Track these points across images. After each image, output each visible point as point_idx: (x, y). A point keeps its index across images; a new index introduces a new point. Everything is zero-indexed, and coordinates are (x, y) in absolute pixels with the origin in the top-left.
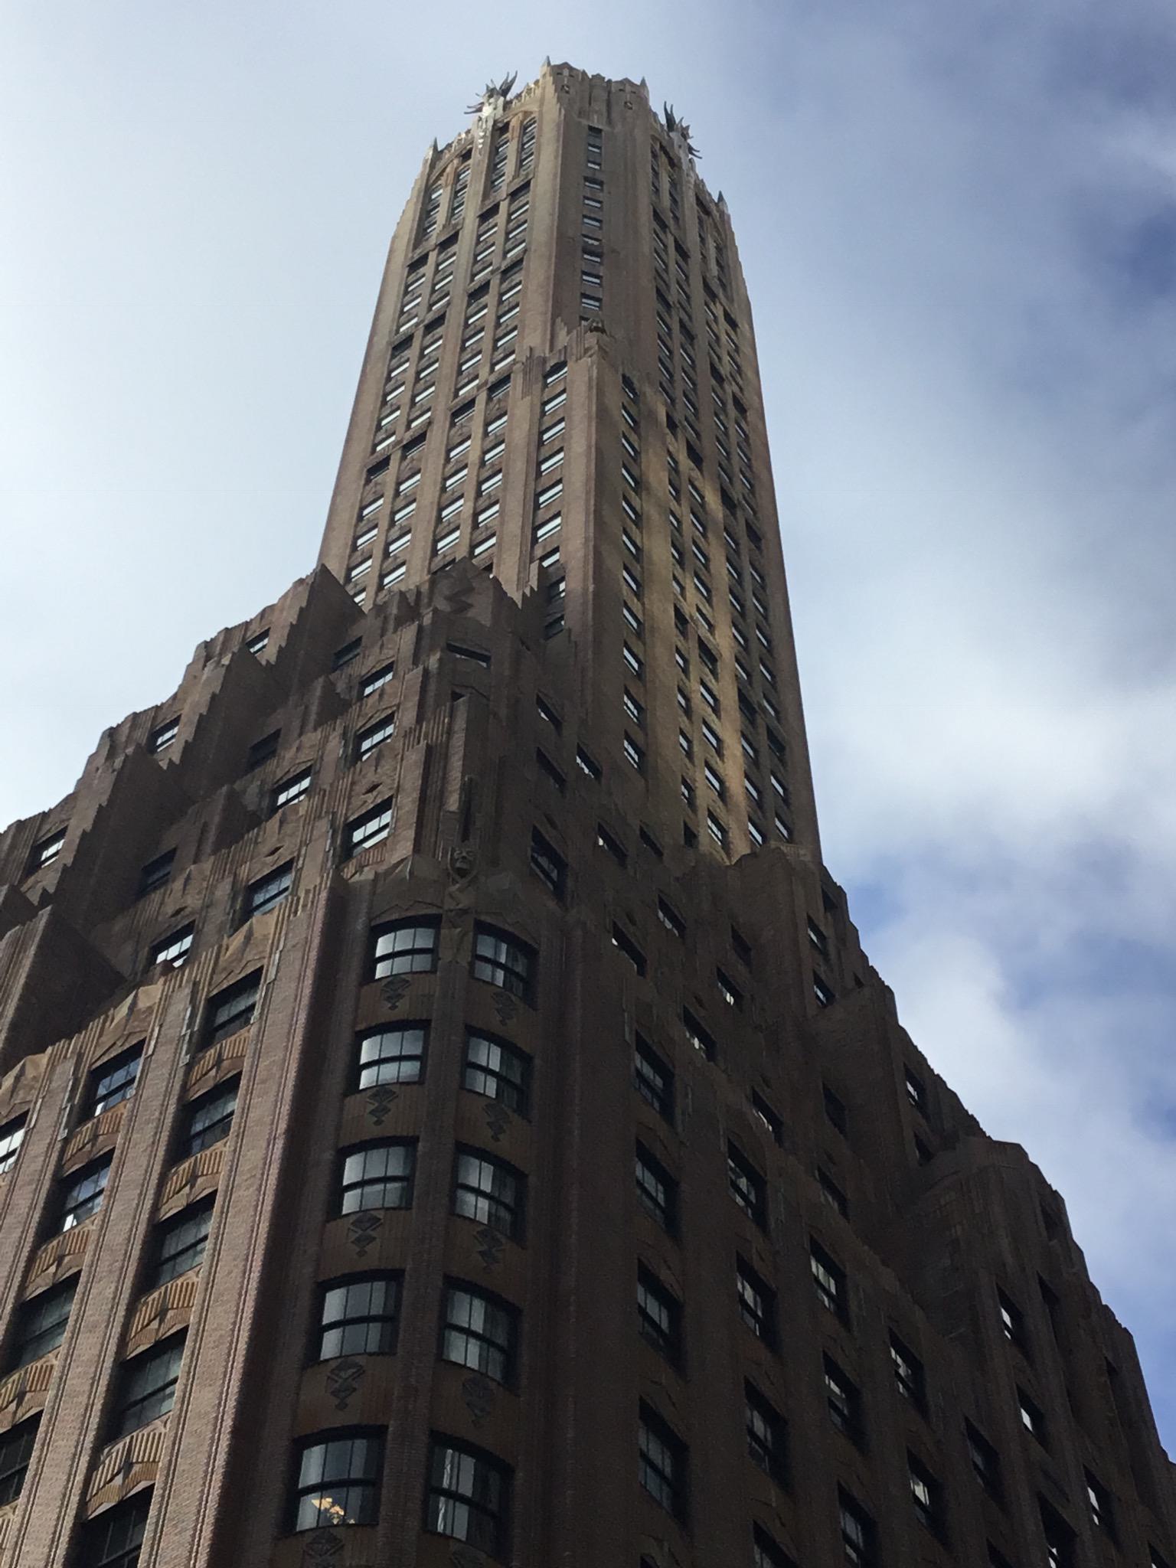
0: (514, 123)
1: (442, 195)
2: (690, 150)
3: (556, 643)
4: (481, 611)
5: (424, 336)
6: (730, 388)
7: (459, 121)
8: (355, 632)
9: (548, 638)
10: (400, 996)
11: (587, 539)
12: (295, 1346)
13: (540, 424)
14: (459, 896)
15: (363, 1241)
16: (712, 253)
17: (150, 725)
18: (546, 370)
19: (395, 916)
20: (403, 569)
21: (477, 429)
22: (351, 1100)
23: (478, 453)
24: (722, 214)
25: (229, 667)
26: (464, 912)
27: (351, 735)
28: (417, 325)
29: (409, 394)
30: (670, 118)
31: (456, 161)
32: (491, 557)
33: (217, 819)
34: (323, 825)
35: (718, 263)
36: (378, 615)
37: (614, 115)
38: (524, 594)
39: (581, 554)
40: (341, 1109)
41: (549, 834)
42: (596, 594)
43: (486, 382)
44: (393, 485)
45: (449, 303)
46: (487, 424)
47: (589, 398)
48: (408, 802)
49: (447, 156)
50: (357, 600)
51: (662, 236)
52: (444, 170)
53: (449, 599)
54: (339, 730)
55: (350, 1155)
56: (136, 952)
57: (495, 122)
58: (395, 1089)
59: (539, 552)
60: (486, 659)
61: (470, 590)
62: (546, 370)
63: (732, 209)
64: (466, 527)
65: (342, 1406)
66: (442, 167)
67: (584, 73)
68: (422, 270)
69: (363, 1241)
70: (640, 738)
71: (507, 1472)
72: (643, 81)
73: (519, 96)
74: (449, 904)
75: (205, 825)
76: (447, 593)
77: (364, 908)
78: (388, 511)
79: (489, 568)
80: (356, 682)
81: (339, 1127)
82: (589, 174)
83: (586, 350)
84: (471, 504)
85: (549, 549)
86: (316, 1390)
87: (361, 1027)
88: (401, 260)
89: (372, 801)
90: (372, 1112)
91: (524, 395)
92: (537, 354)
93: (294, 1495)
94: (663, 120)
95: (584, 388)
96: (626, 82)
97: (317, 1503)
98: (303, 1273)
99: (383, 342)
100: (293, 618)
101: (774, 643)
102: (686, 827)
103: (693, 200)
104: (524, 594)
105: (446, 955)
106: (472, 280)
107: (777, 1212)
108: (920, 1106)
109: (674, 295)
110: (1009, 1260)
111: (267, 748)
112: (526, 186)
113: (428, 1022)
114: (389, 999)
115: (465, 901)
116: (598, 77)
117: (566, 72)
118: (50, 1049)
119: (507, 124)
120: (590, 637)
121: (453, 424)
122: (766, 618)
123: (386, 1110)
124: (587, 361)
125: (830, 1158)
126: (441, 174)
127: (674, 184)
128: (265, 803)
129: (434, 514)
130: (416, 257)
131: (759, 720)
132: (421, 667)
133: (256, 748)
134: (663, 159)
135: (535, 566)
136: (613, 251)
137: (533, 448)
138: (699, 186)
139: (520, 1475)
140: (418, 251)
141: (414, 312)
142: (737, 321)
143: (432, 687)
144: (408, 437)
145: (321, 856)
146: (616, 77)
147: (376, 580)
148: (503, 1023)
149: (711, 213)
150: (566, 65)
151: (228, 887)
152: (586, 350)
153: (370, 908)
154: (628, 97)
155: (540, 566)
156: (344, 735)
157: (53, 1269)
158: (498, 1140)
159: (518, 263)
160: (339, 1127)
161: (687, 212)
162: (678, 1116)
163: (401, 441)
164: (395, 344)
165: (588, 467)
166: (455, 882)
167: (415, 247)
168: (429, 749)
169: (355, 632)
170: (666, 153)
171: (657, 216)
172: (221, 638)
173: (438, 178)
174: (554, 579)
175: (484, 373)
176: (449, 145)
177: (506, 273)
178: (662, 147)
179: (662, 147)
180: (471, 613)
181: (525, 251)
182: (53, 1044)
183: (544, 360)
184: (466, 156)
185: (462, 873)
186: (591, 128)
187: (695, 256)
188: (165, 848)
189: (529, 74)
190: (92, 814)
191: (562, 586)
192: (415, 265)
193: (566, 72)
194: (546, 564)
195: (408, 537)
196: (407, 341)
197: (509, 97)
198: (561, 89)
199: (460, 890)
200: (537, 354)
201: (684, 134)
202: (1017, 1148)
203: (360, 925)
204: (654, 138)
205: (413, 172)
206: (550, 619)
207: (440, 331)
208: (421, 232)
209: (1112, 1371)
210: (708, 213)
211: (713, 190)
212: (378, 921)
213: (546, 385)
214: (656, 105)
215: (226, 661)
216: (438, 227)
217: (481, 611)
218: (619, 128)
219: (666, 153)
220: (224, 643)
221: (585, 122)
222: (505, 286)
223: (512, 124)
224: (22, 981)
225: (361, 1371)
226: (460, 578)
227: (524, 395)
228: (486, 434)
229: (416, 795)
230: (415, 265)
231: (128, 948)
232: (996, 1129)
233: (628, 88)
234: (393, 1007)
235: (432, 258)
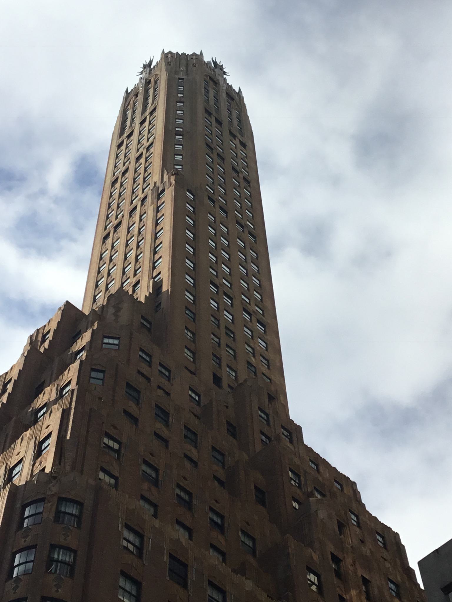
0: (152, 80)
1: (129, 113)
7: (132, 80)
26: (53, 495)
38: (150, 293)
39: (167, 275)
43: (141, 198)
44: (111, 244)
49: (131, 95)
51: (209, 118)
52: (130, 102)
53: (114, 307)
57: (146, 80)
63: (245, 95)
72: (201, 52)
74: (49, 493)
76: (113, 304)
84: (135, 253)
87: (14, 550)
88: (115, 144)
102: (214, 375)
104: (150, 293)
106: (114, 175)
112: (155, 109)
115: (55, 490)
116: (184, 54)
117: (169, 56)
119: (150, 80)
125: (247, 523)
126: (129, 104)
130: (120, 142)
134: (211, 83)
135: (152, 281)
146: (190, 53)
148: (65, 539)
154: (195, 60)
155: (154, 282)
158: (58, 591)
161: (222, 104)
167: (120, 137)
171: (207, 111)
172: (35, 334)
173: (128, 106)
176: (132, 90)
178: (211, 78)
179: (211, 78)
184: (137, 95)
189: (157, 58)
192: (120, 146)
193: (169, 56)
194: (156, 280)
198: (168, 64)
199: (53, 486)
203: (18, 505)
210: (232, 99)
212: (25, 503)
216: (149, 105)
221: (177, 77)
230: (120, 146)
233: (194, 57)
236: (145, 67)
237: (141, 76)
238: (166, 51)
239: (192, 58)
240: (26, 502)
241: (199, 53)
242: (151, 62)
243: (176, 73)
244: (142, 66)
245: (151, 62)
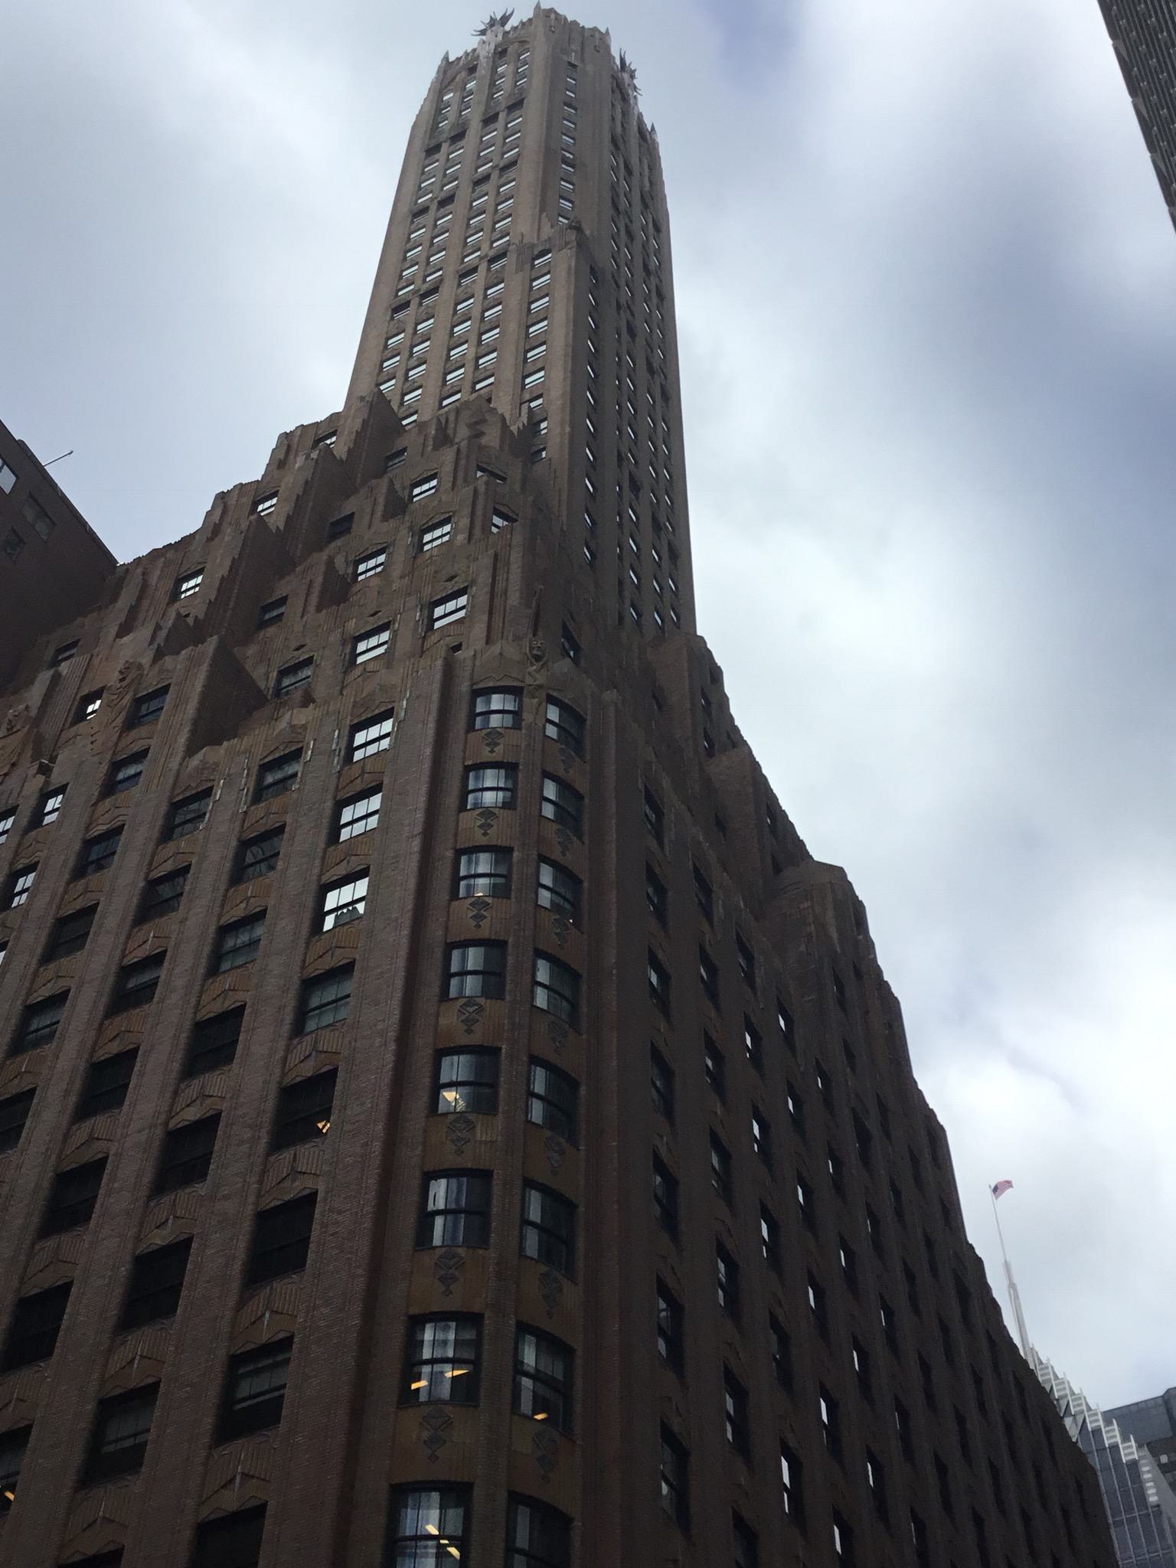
4: (491, 438)
6: (653, 280)
9: (533, 463)
15: (479, 917)
17: (251, 494)
18: (530, 255)
19: (491, 684)
20: (419, 392)
21: (479, 290)
23: (480, 309)
24: (654, 142)
26: (540, 687)
27: (416, 529)
29: (425, 254)
30: (622, 60)
34: (412, 601)
36: (420, 432)
39: (559, 403)
41: (571, 626)
45: (457, 186)
46: (487, 289)
48: (481, 591)
50: (404, 423)
53: (469, 426)
58: (496, 811)
59: (527, 397)
60: (504, 479)
61: (483, 421)
62: (530, 255)
64: (470, 366)
65: (469, 1031)
66: (452, 74)
70: (593, 547)
71: (574, 1085)
73: (515, 29)
74: (529, 680)
77: (467, 674)
79: (489, 400)
80: (408, 483)
81: (456, 835)
83: (567, 243)
90: (480, 827)
91: (517, 271)
93: (437, 1088)
94: (618, 62)
95: (564, 274)
96: (595, 29)
99: (404, 209)
103: (636, 129)
107: (719, 910)
111: (343, 526)
115: (541, 679)
116: (575, 23)
117: (553, 16)
120: (566, 466)
121: (459, 285)
127: (624, 114)
128: (350, 570)
131: (663, 536)
132: (472, 487)
133: (334, 524)
137: (524, 314)
138: (640, 117)
143: (481, 502)
144: (424, 288)
149: (646, 139)
150: (552, 10)
154: (595, 42)
157: (243, 905)
159: (513, 163)
162: (666, 840)
164: (412, 213)
166: (532, 665)
174: (538, 418)
175: (485, 247)
176: (459, 59)
177: (505, 169)
180: (484, 441)
181: (518, 154)
183: (532, 246)
185: (537, 658)
186: (570, 63)
188: (276, 596)
189: (523, 13)
190: (228, 563)
193: (553, 16)
194: (533, 405)
195: (424, 367)
196: (424, 210)
197: (508, 27)
198: (550, 30)
199: (538, 671)
201: (632, 77)
202: (841, 870)
203: (464, 687)
205: (428, 74)
207: (449, 207)
208: (434, 127)
211: (648, 122)
212: (481, 686)
213: (533, 266)
214: (615, 52)
215: (314, 455)
217: (491, 438)
220: (301, 436)
222: (503, 180)
225: (481, 1009)
227: (517, 271)
228: (485, 296)
234: (492, 751)
235: (445, 147)
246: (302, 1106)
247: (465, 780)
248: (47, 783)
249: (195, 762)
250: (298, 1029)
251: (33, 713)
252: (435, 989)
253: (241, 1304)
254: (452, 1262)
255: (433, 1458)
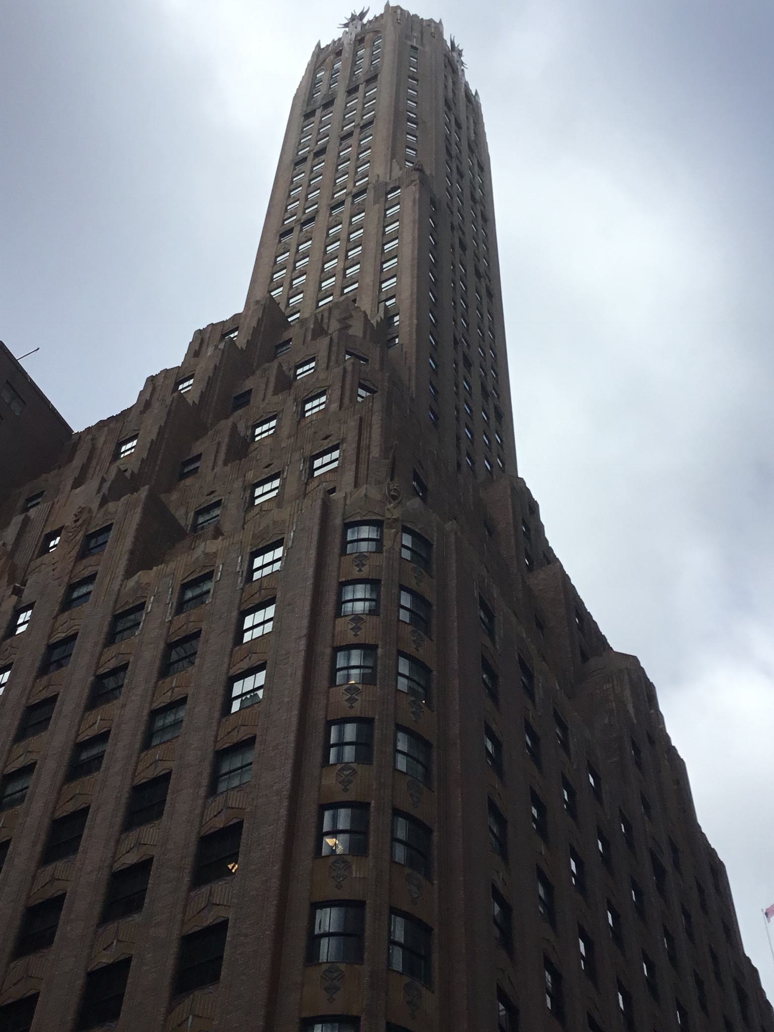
2: (462, 63)
3: (392, 352)
4: (357, 329)
5: (314, 159)
6: (479, 207)
8: (286, 336)
10: (364, 565)
11: (412, 294)
12: (317, 756)
13: (384, 221)
14: (393, 512)
16: (472, 127)
19: (359, 518)
22: (339, 621)
25: (223, 351)
26: (396, 520)
28: (309, 152)
30: (452, 43)
31: (332, 57)
32: (355, 295)
33: (226, 440)
35: (475, 133)
36: (301, 327)
37: (424, 41)
40: (334, 626)
42: (418, 325)
47: (414, 211)
48: (350, 447)
53: (340, 321)
54: (292, 398)
55: (340, 651)
56: (187, 513)
58: (364, 617)
66: (323, 58)
67: (409, 13)
68: (312, 119)
69: (351, 700)
71: (429, 831)
74: (388, 515)
75: (219, 443)
77: (341, 511)
78: (292, 261)
79: (354, 301)
81: (333, 636)
82: (411, 74)
85: (389, 296)
86: (330, 780)
89: (326, 444)
92: (381, 179)
94: (449, 44)
95: (411, 204)
96: (431, 21)
97: (330, 841)
98: (318, 714)
99: (289, 158)
100: (254, 324)
101: (498, 357)
103: (463, 94)
105: (387, 544)
107: (539, 693)
108: (580, 627)
109: (454, 150)
110: (635, 721)
111: (243, 400)
113: (379, 581)
114: (357, 566)
115: (397, 514)
116: (416, 16)
117: (399, 11)
118: (155, 568)
122: (467, 330)
123: (359, 629)
124: (412, 188)
128: (249, 432)
129: (321, 266)
136: (424, 122)
138: (466, 85)
139: (435, 834)
140: (310, 107)
141: (307, 143)
142: (483, 167)
145: (298, 473)
147: (285, 300)
150: (398, 7)
151: (241, 484)
152: (413, 181)
153: (344, 513)
154: (432, 29)
156: (295, 399)
157: (169, 694)
160: (333, 636)
163: (299, 220)
165: (413, 251)
168: (361, 419)
169: (286, 336)
170: (451, 64)
176: (328, 46)
181: (374, 116)
182: (157, 565)
183: (386, 184)
184: (339, 53)
185: (394, 498)
186: (412, 47)
187: (464, 127)
190: (155, 430)
191: (397, 318)
192: (309, 115)
199: (394, 508)
200: (381, 179)
202: (635, 658)
203: (338, 522)
204: (445, 55)
206: (390, 337)
209: (677, 782)
214: (447, 37)
215: (221, 346)
217: (357, 329)
218: (428, 49)
219: (451, 64)
221: (409, 43)
223: (366, 38)
224: (134, 526)
226: (347, 308)
229: (354, 445)
230: (309, 115)
231: (182, 511)
232: (618, 644)
236: (353, 18)
237: (347, 29)
238: (392, 4)
239: (429, 26)
240: (352, 520)
241: (438, 21)
242: (363, 15)
243: (408, 37)
244: (349, 16)
245: (363, 15)
246: (216, 850)
247: (340, 594)
248: (19, 602)
249: (131, 583)
250: (212, 790)
251: (9, 548)
252: (337, 550)
253: (170, 1011)
254: (335, 975)
255: (351, 707)
